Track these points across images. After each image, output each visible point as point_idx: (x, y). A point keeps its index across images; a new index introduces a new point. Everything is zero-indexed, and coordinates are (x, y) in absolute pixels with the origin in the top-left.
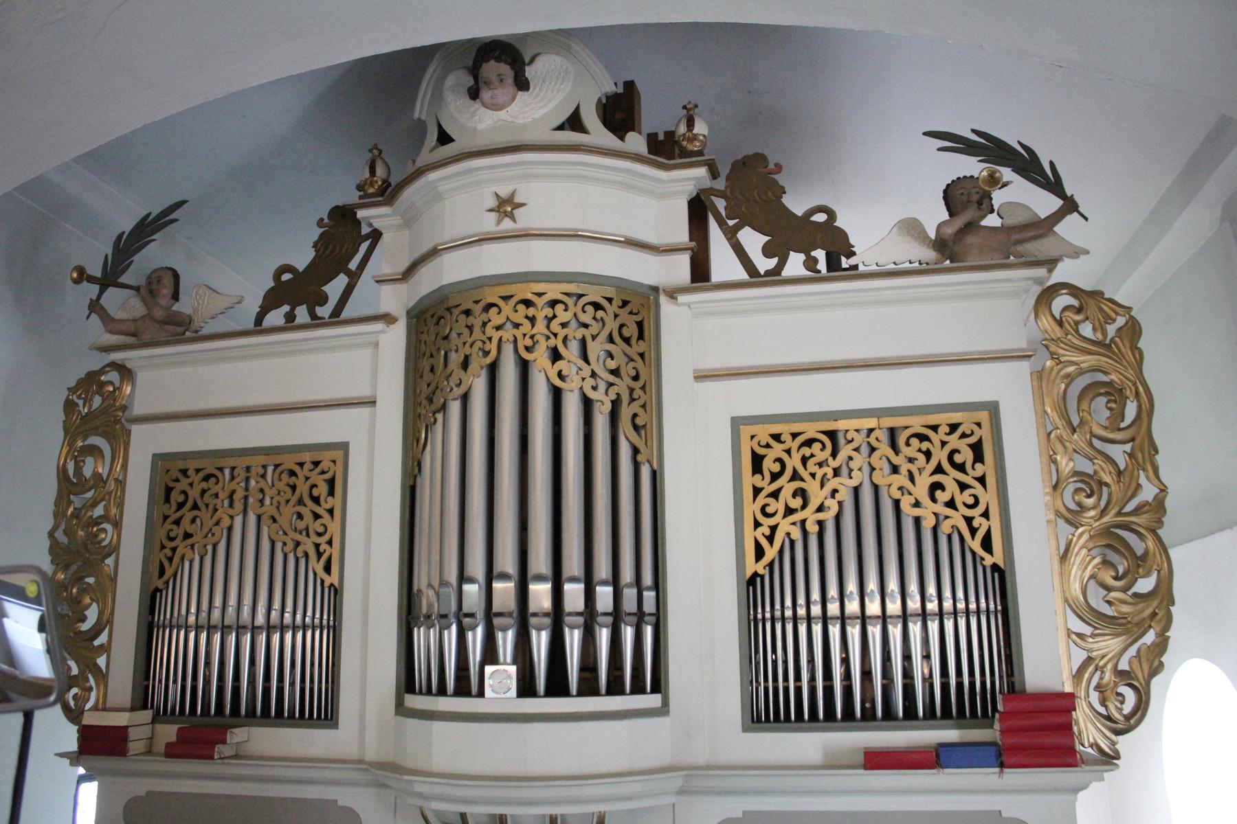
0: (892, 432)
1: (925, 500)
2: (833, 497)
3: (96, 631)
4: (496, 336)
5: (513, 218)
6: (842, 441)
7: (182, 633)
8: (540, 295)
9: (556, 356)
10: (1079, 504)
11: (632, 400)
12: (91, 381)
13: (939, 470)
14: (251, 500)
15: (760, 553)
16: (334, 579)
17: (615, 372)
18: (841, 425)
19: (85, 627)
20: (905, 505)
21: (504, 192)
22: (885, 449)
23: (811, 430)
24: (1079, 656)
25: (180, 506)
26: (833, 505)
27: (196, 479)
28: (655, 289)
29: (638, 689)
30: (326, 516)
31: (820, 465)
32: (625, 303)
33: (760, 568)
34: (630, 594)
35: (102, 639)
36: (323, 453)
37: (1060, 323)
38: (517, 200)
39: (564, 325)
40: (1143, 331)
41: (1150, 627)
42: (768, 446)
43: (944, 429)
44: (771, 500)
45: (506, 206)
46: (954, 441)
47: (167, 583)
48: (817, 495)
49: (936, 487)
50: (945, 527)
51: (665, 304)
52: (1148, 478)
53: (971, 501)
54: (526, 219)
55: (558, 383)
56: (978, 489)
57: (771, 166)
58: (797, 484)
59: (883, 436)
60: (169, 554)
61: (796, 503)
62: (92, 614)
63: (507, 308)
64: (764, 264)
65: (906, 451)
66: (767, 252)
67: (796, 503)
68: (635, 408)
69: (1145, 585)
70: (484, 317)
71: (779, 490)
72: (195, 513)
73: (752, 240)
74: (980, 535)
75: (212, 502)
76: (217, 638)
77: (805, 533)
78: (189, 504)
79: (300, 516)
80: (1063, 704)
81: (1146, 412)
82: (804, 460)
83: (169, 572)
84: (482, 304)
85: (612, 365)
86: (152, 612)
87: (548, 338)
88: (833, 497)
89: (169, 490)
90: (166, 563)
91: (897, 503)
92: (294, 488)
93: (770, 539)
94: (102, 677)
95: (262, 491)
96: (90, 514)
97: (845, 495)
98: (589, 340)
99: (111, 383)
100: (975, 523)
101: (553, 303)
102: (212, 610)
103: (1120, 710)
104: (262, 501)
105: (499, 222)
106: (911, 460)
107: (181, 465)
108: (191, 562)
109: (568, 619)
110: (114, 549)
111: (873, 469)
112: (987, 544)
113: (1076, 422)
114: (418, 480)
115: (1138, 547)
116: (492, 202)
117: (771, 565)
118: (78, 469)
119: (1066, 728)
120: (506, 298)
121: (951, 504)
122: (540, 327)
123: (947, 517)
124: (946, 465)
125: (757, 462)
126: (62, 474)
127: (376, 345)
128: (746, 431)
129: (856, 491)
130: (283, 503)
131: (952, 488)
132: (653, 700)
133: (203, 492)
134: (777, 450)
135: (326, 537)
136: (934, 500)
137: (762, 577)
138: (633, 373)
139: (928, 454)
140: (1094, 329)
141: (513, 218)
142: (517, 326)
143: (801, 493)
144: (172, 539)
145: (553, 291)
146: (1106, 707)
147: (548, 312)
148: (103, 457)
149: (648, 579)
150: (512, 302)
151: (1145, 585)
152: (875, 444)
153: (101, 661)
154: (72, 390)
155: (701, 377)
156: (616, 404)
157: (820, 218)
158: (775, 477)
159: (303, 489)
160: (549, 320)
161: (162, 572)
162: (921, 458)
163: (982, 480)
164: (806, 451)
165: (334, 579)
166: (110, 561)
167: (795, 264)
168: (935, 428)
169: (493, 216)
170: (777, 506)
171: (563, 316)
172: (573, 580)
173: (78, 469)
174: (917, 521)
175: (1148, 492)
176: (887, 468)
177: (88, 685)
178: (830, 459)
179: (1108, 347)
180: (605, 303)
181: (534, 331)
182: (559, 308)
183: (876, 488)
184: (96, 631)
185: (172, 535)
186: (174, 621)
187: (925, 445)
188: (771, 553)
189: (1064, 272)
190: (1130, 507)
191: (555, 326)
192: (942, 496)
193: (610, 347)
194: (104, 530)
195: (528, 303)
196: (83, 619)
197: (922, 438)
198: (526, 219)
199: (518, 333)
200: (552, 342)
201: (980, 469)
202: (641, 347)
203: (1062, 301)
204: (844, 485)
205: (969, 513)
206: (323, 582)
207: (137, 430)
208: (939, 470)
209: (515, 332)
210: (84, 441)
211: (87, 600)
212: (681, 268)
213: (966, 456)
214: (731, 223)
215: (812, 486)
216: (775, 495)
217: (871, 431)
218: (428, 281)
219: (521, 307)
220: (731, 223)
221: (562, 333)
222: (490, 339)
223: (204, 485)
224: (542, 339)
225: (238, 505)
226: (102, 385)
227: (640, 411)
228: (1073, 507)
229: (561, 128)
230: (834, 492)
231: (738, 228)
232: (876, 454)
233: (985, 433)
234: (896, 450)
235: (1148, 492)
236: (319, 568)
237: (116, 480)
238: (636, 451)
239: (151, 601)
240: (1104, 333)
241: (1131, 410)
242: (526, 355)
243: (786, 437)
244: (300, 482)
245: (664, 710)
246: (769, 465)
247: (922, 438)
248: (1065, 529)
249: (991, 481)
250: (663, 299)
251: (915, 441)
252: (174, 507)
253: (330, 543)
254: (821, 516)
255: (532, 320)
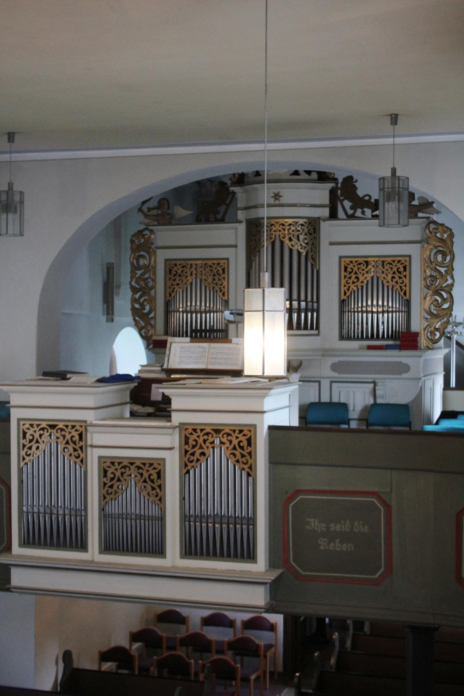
0: (383, 262)
1: (390, 281)
2: (365, 279)
3: (150, 312)
4: (274, 233)
5: (279, 200)
6: (369, 263)
7: (178, 314)
8: (286, 222)
9: (290, 240)
10: (431, 284)
11: (311, 251)
12: (140, 232)
13: (394, 273)
14: (198, 274)
15: (345, 293)
16: (226, 298)
17: (307, 244)
18: (369, 259)
19: (145, 311)
20: (385, 282)
21: (276, 191)
22: (380, 267)
23: (361, 260)
24: (426, 324)
25: (175, 275)
26: (365, 281)
27: (179, 267)
28: (319, 218)
29: (312, 328)
30: (404, 278)
31: (363, 270)
32: (310, 223)
33: (345, 298)
34: (310, 304)
35: (152, 315)
36: (220, 261)
37: (431, 233)
38: (281, 194)
39: (293, 231)
40: (455, 236)
41: (445, 317)
42: (349, 264)
43: (396, 262)
44: (349, 280)
45: (277, 196)
46: (399, 265)
47: (172, 299)
48: (361, 278)
49: (393, 277)
50: (395, 289)
51: (323, 224)
52: (450, 278)
53: (402, 282)
54: (283, 200)
55: (291, 247)
56: (404, 279)
57: (354, 180)
58: (356, 275)
59: (381, 263)
60: (172, 289)
61: (356, 280)
62: (147, 308)
63: (277, 226)
64: (350, 212)
65: (386, 267)
66: (351, 208)
67: (180, 282)
68: (313, 253)
69: (446, 306)
70: (271, 228)
71: (195, 452)
72: (37, 445)
73: (347, 204)
74: (403, 291)
75: (185, 274)
76: (189, 315)
77: (358, 289)
78: (354, 272)
79: (214, 279)
80: (417, 335)
81: (452, 259)
82: (358, 269)
83: (173, 295)
84: (270, 224)
85: (306, 241)
86: (168, 307)
87: (288, 235)
88: (365, 279)
89: (170, 271)
90: (171, 293)
91: (382, 281)
92: (212, 271)
93: (348, 290)
94: (154, 327)
95: (201, 271)
96: (144, 277)
97: (369, 279)
98: (300, 235)
99: (146, 235)
100: (402, 288)
101: (290, 225)
102: (187, 307)
103: (434, 338)
104: (201, 275)
105: (275, 201)
106: (387, 270)
107: (174, 262)
108: (179, 293)
109: (293, 311)
110: (154, 287)
111: (377, 272)
112: (405, 294)
113: (432, 260)
114: (251, 270)
115: (445, 295)
116: (272, 195)
117: (348, 297)
118: (138, 262)
119: (416, 341)
120: (277, 223)
121: (217, 284)
122: (286, 232)
123: (395, 286)
124: (396, 272)
125: (105, 472)
126: (132, 264)
127: (237, 229)
128: (343, 260)
129: (372, 278)
130: (208, 276)
131: (397, 278)
132: (315, 332)
133: (182, 271)
134: (351, 266)
135: (223, 286)
136: (392, 281)
137: (346, 300)
138: (312, 243)
139: (392, 269)
140: (440, 235)
141: (279, 200)
142: (280, 231)
143: (357, 278)
144: (173, 285)
145: (290, 221)
146: (431, 337)
147: (289, 227)
148: (146, 258)
149: (315, 299)
150: (279, 224)
151: (446, 306)
152: (378, 265)
153: (152, 322)
154: (133, 236)
155: (332, 244)
156: (307, 253)
157: (367, 198)
158: (350, 273)
159: (215, 271)
160: (289, 230)
161: (170, 295)
162: (390, 270)
163: (405, 276)
164: (359, 266)
165: (226, 298)
166: (153, 292)
167: (359, 213)
168: (394, 261)
169: (273, 199)
170: (351, 281)
171: (293, 228)
172: (295, 300)
173: (138, 262)
174: (388, 286)
175: (450, 281)
176: (381, 272)
177: (148, 329)
178: (365, 269)
179: (444, 240)
180: (213, 265)
181: (284, 233)
182: (292, 226)
183: (378, 278)
184: (150, 312)
185: (173, 284)
186: (175, 310)
187: (391, 266)
188: (348, 294)
189: (435, 217)
190: (444, 285)
191: (290, 231)
192: (395, 280)
193: (306, 237)
194: (149, 282)
195: (283, 225)
196: (145, 309)
197: (390, 264)
198: (283, 200)
199: (280, 233)
200: (290, 236)
201: (405, 273)
202: (315, 235)
203: (432, 226)
204: (369, 276)
205: (401, 285)
206: (222, 299)
207: (159, 252)
208: (394, 273)
209: (279, 233)
210: (139, 253)
211: (145, 303)
212: (326, 212)
213: (402, 269)
214: (342, 198)
215: (360, 276)
216: (350, 278)
217: (377, 261)
218: (254, 214)
219: (281, 226)
220: (342, 198)
221: (292, 233)
222: (272, 234)
223: (182, 269)
224: (287, 235)
225: (194, 276)
226: (143, 236)
227: (313, 254)
228: (429, 284)
229: (291, 175)
230: (366, 278)
231: (343, 200)
232: (378, 268)
233: (407, 263)
234: (383, 267)
235: (450, 281)
236: (221, 295)
237: (152, 267)
238: (312, 265)
239: (167, 304)
240: (443, 236)
241: (448, 258)
242: (283, 240)
243: (354, 262)
244: (214, 269)
245: (318, 335)
246: (349, 270)
247: (390, 264)
248: (426, 290)
249: (408, 277)
250: (321, 222)
251: (388, 265)
252: (173, 276)
253: (224, 287)
254: (362, 284)
255: (284, 230)
